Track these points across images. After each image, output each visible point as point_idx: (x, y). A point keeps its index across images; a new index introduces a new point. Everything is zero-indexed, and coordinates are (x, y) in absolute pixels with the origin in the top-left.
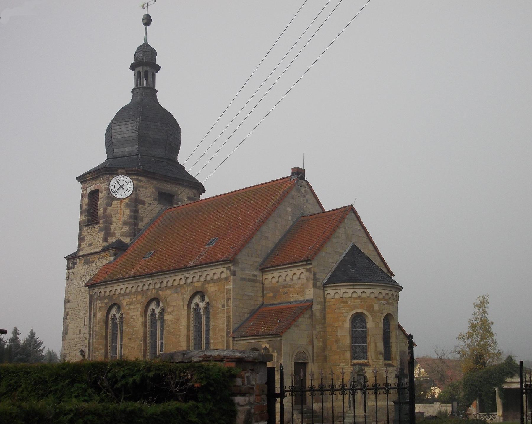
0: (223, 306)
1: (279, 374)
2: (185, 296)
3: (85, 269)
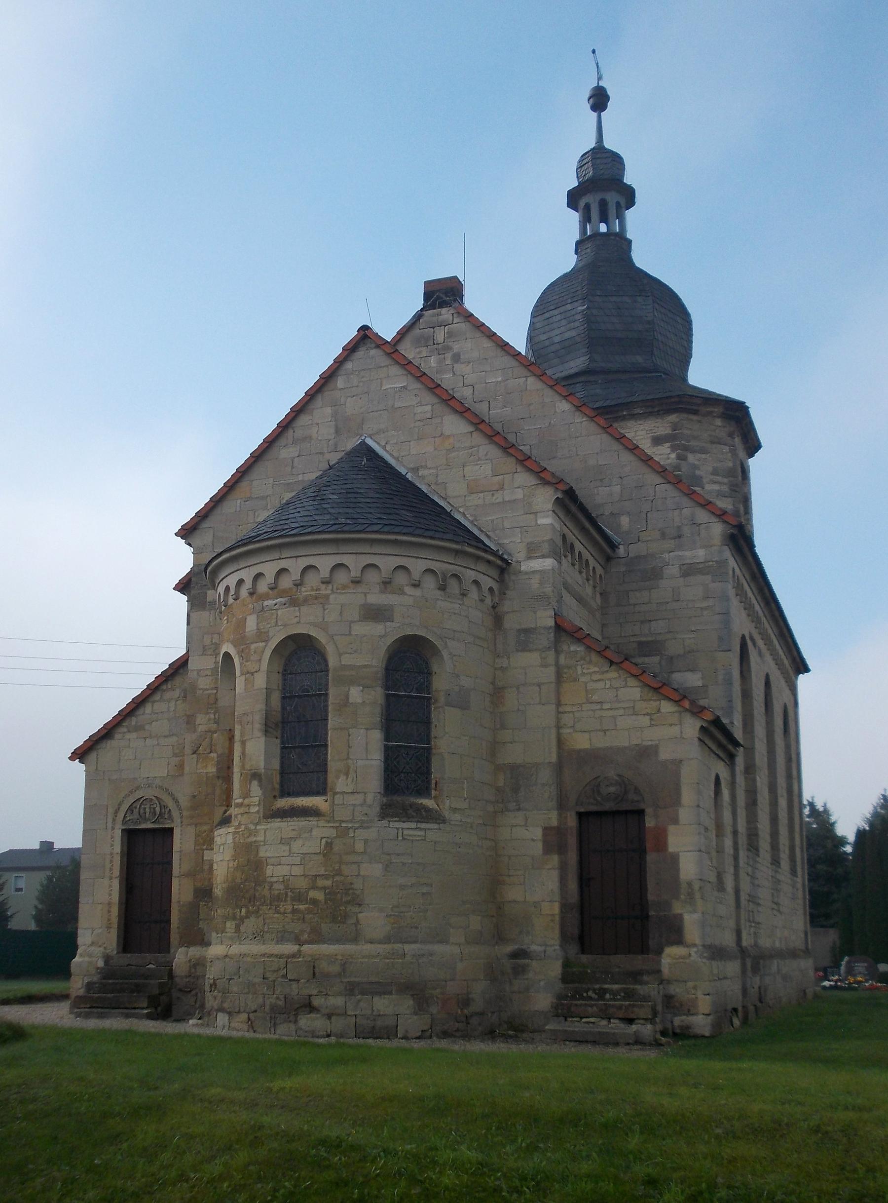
1: (177, 867)
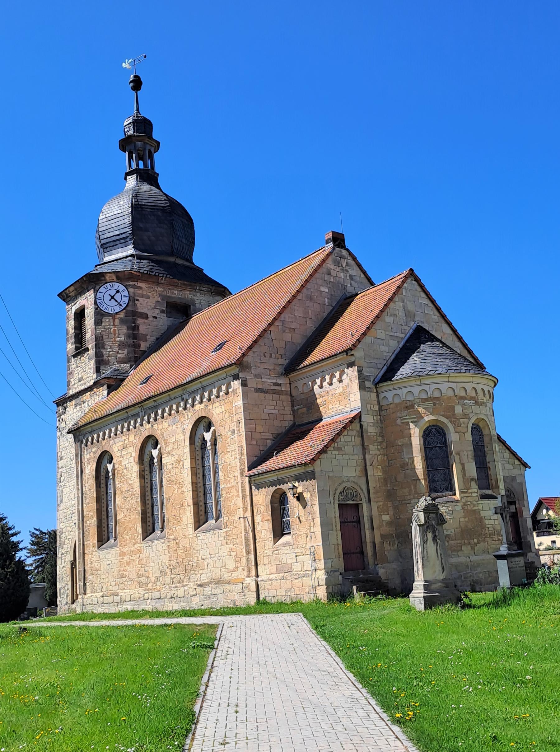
0: (233, 433)
2: (185, 427)
3: (77, 413)
